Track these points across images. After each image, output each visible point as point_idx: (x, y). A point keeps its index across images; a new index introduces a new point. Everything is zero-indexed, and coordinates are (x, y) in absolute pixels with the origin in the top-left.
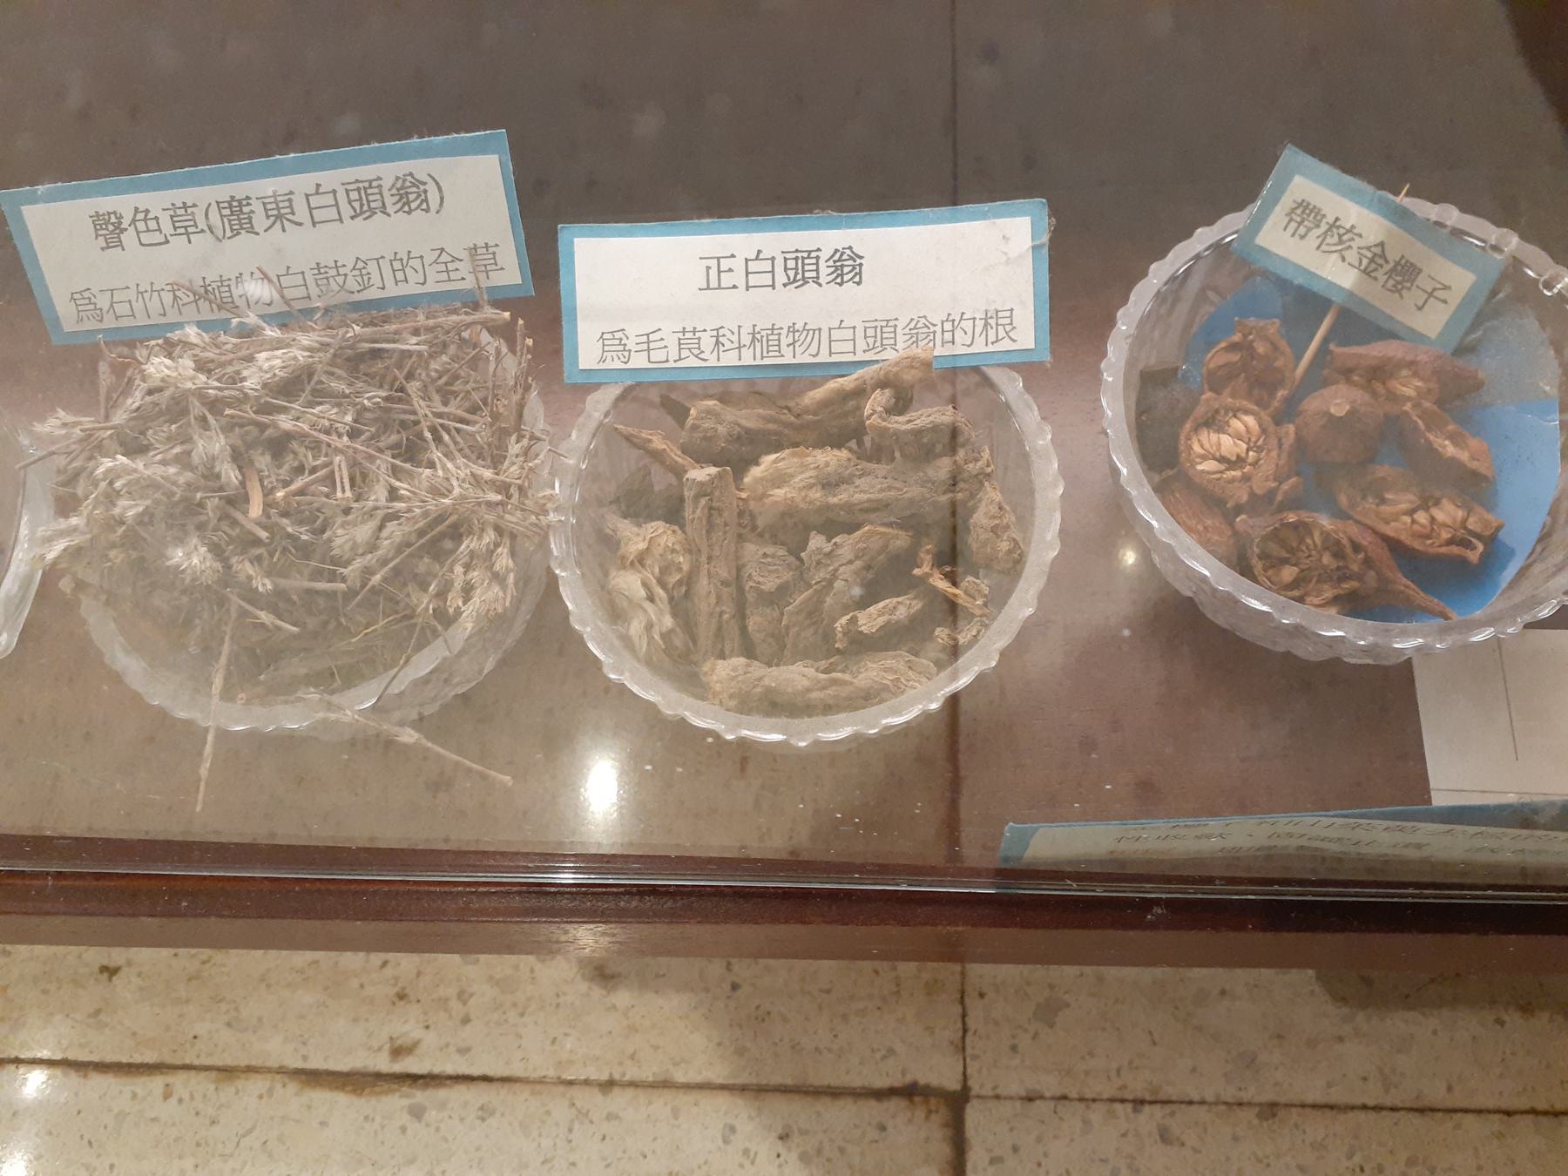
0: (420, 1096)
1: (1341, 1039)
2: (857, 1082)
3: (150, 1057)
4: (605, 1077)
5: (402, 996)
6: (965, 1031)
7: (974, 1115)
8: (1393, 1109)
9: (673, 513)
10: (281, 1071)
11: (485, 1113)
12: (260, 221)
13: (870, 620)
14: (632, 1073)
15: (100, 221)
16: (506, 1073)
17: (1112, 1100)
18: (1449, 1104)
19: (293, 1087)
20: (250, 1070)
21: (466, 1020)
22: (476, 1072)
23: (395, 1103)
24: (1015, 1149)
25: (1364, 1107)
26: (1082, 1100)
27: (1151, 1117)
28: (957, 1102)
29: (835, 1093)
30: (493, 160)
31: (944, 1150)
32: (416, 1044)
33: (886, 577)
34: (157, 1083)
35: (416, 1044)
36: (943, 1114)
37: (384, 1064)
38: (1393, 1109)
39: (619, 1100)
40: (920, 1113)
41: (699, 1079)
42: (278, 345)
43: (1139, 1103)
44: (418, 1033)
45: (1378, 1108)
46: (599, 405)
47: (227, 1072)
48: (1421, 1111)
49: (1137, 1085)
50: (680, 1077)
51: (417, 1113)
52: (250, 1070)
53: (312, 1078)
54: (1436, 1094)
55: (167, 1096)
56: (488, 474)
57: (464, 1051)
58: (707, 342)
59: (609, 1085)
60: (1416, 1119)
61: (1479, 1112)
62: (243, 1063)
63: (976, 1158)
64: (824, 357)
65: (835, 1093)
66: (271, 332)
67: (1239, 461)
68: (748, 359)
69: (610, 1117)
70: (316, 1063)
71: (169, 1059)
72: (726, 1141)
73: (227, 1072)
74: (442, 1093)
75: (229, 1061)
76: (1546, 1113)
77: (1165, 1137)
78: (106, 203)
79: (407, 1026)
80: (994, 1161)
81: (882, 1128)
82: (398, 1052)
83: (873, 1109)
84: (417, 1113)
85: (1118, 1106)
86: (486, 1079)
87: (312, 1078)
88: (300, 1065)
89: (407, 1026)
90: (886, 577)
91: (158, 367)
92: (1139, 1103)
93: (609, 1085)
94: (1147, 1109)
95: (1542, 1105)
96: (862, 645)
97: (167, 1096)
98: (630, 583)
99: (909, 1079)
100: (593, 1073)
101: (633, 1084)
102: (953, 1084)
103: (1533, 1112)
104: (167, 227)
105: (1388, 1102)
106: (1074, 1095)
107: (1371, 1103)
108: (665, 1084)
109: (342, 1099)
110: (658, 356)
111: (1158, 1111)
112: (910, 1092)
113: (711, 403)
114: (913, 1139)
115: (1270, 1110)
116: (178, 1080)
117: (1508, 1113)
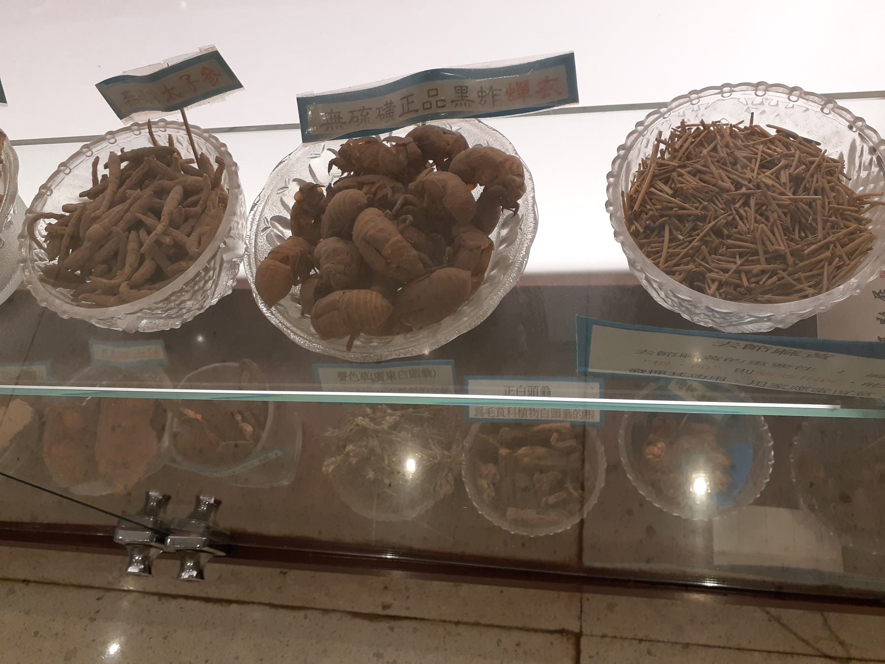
0: (393, 623)
1: (713, 623)
2: (543, 627)
3: (299, 604)
4: (456, 620)
5: (386, 588)
6: (582, 611)
7: (584, 641)
8: (730, 648)
9: (496, 462)
10: (344, 612)
11: (415, 630)
12: (386, 377)
13: (552, 499)
14: (466, 619)
15: (339, 374)
16: (422, 617)
17: (632, 639)
18: (749, 647)
19: (349, 617)
20: (334, 611)
21: (408, 598)
22: (412, 615)
23: (384, 625)
24: (598, 653)
25: (719, 647)
26: (621, 638)
27: (645, 646)
28: (577, 637)
29: (536, 631)
30: (450, 367)
31: (572, 652)
32: (391, 605)
33: (558, 486)
34: (302, 613)
35: (391, 605)
36: (572, 640)
37: (380, 611)
38: (730, 648)
39: (461, 628)
40: (565, 640)
41: (489, 623)
42: (391, 415)
43: (641, 640)
44: (392, 601)
45: (723, 648)
46: (475, 428)
47: (326, 611)
48: (739, 649)
49: (640, 635)
50: (482, 621)
51: (392, 629)
52: (334, 611)
53: (355, 615)
54: (745, 644)
55: (306, 618)
56: (446, 453)
57: (407, 609)
58: (506, 412)
59: (457, 623)
60: (737, 652)
61: (759, 651)
62: (331, 608)
63: (584, 656)
64: (539, 418)
65: (536, 631)
66: (389, 411)
67: (659, 456)
68: (517, 417)
69: (458, 634)
70: (356, 610)
71: (305, 605)
72: (498, 645)
73: (326, 611)
74: (400, 623)
75: (326, 607)
76: (782, 653)
77: (649, 653)
78: (342, 370)
79: (388, 598)
80: (591, 657)
81: (552, 644)
82: (385, 607)
83: (548, 636)
84: (392, 629)
85: (634, 642)
86: (415, 619)
87: (355, 615)
88: (350, 610)
89: (388, 598)
90: (558, 486)
91: (360, 420)
92: (641, 640)
93: (457, 623)
94: (644, 643)
95: (781, 650)
96: (549, 506)
97: (306, 618)
98: (484, 483)
99: (561, 627)
100: (452, 619)
101: (466, 623)
102: (577, 630)
103: (778, 652)
104: (359, 377)
105: (728, 645)
106: (619, 635)
107: (722, 645)
108: (477, 624)
109: (366, 622)
110: (492, 415)
111: (647, 644)
112: (562, 632)
113: (507, 429)
114: (562, 649)
115: (687, 646)
116: (309, 612)
117: (770, 652)
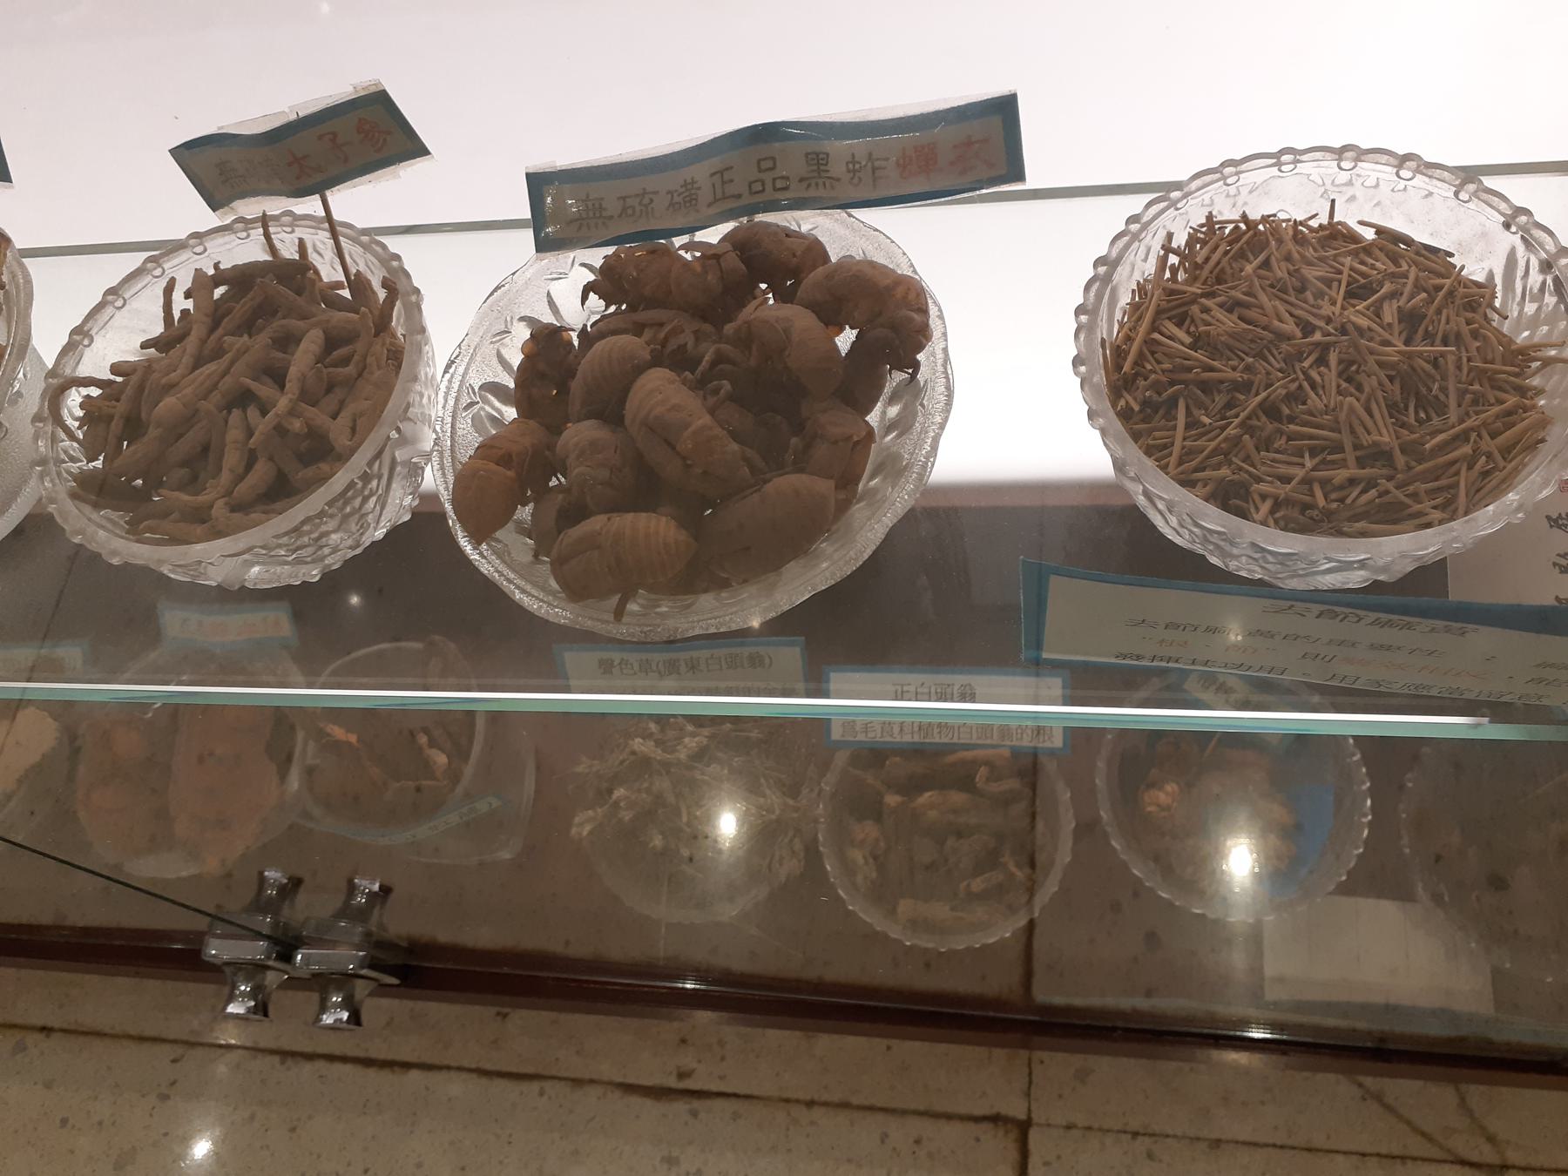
0: (697, 1104)
1: (1263, 1103)
2: (963, 1110)
3: (530, 1070)
4: (808, 1098)
5: (683, 1041)
6: (1030, 1083)
7: (1034, 1136)
8: (1294, 1148)
9: (878, 818)
10: (610, 1083)
11: (736, 1116)
12: (683, 668)
13: (978, 885)
14: (825, 1097)
15: (601, 662)
16: (748, 1092)
17: (1119, 1132)
18: (1326, 1147)
19: (618, 1093)
20: (592, 1081)
21: (723, 1059)
22: (729, 1090)
23: (681, 1107)
24: (1059, 1157)
25: (1274, 1146)
26: (1100, 1129)
27: (1142, 1144)
28: (1023, 1129)
29: (949, 1117)
30: (797, 650)
31: (1013, 1154)
32: (693, 1071)
33: (990, 860)
34: (535, 1086)
35: (693, 1071)
36: (1014, 1134)
37: (673, 1082)
38: (1294, 1148)
39: (817, 1113)
40: (1001, 1133)
41: (867, 1103)
42: (693, 735)
43: (1135, 1134)
44: (695, 1065)
45: (1282, 1147)
46: (841, 759)
47: (577, 1082)
48: (1309, 1150)
49: (1135, 1125)
50: (855, 1101)
51: (694, 1114)
52: (592, 1081)
53: (629, 1088)
54: (1319, 1141)
55: (541, 1094)
56: (791, 802)
57: (721, 1078)
58: (896, 730)
59: (810, 1104)
60: (1305, 1154)
61: (1345, 1153)
62: (587, 1076)
63: (1034, 1161)
64: (955, 740)
65: (949, 1117)
66: (690, 728)
67: (1168, 808)
68: (916, 739)
69: (812, 1123)
70: (631, 1080)
71: (541, 1071)
72: (883, 1142)
73: (577, 1082)
74: (709, 1103)
75: (578, 1075)
76: (1386, 1156)
77: (1150, 1156)
78: (605, 655)
79: (687, 1060)
80: (1046, 1164)
81: (978, 1140)
82: (682, 1075)
83: (971, 1126)
84: (694, 1114)
85: (1124, 1137)
86: (736, 1096)
87: (629, 1088)
88: (620, 1080)
89: (687, 1060)
90: (990, 860)
91: (637, 744)
92: (1135, 1134)
93: (810, 1104)
94: (1140, 1138)
95: (1384, 1151)
96: (972, 897)
97: (541, 1094)
98: (857, 856)
99: (994, 1111)
100: (801, 1095)
101: (826, 1104)
102: (1022, 1116)
103: (1378, 1155)
104: (636, 667)
105: (1290, 1142)
106: (1096, 1126)
107: (1279, 1143)
108: (845, 1105)
109: (648, 1102)
110: (871, 735)
111: (1147, 1140)
112: (995, 1119)
113: (897, 759)
114: (997, 1149)
115: (1217, 1143)
116: (547, 1085)
117: (1364, 1155)
